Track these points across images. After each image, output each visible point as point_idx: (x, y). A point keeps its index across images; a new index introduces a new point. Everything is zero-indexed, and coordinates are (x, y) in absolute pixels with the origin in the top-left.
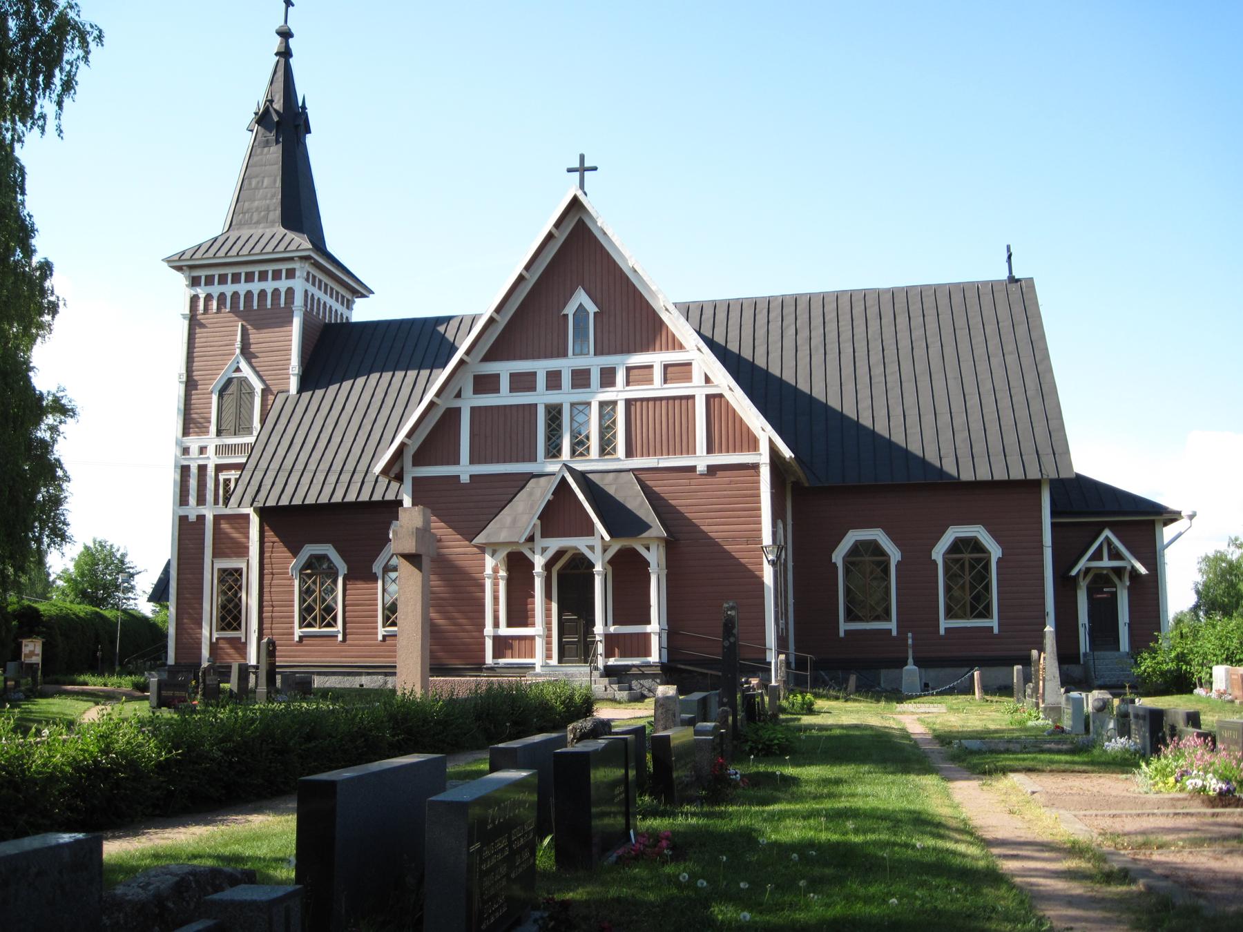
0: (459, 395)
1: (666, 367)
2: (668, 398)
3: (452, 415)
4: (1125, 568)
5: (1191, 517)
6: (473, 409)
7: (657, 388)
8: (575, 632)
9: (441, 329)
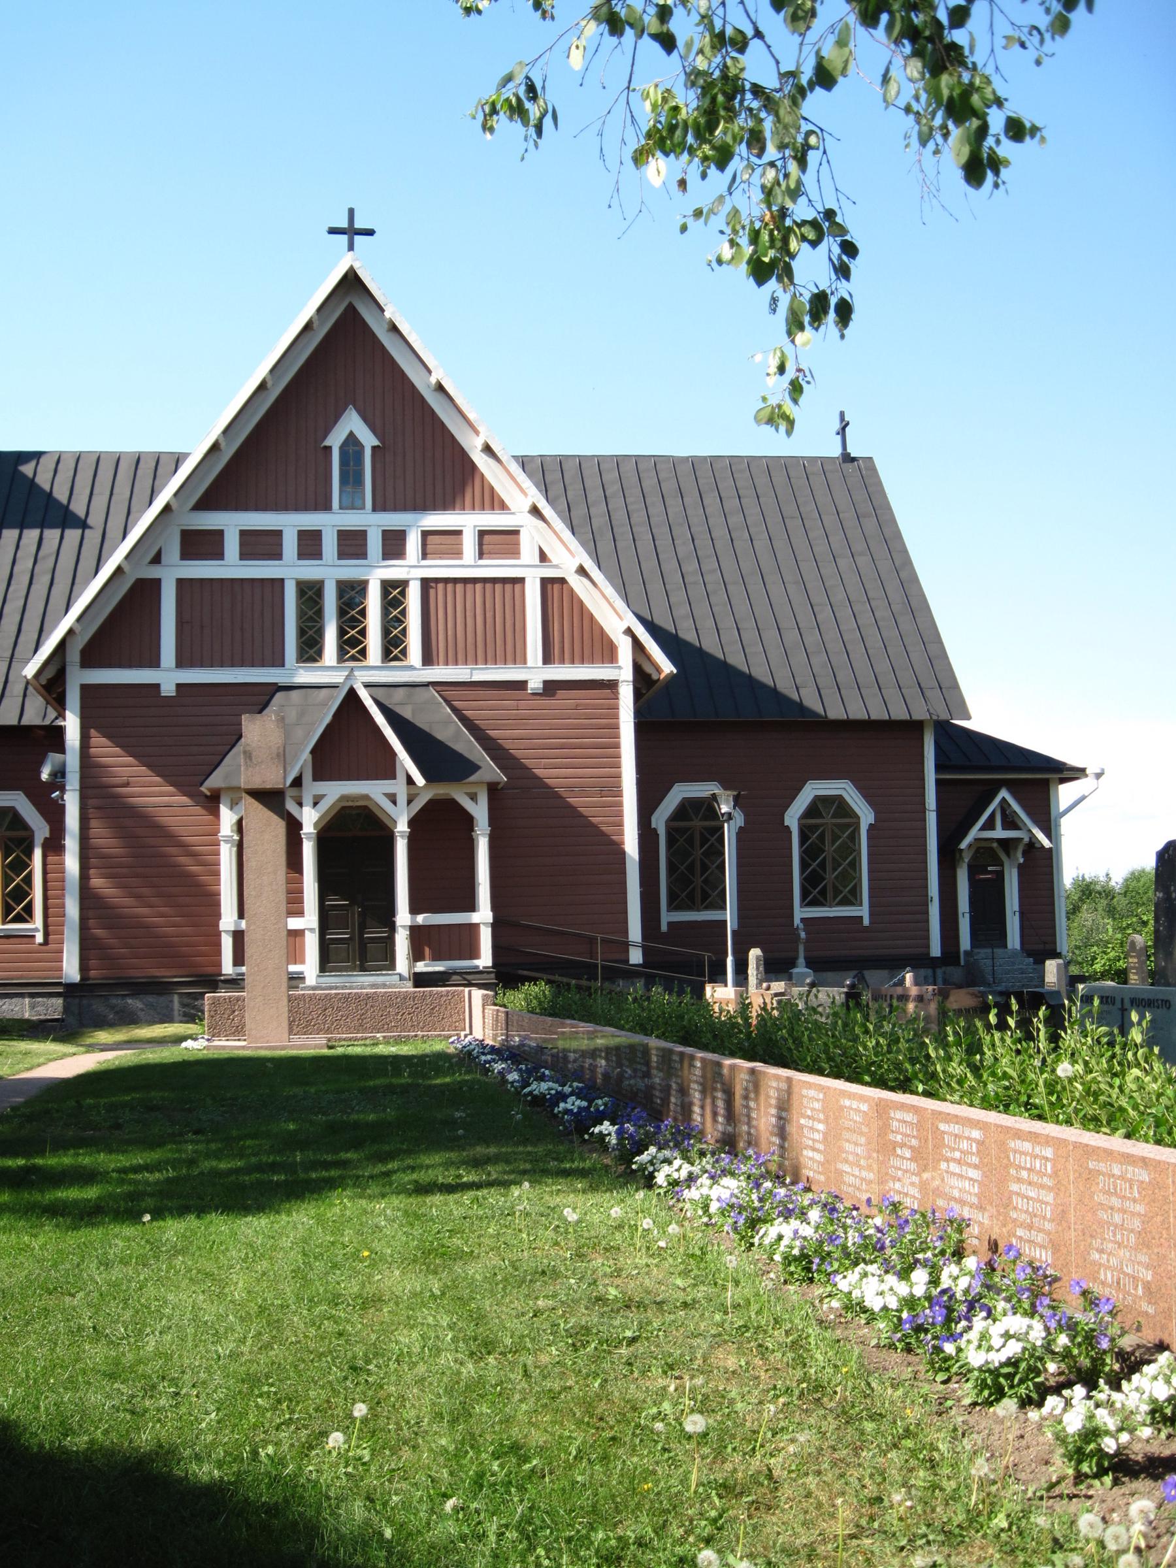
0: (157, 560)
1: (482, 534)
2: (485, 580)
3: (147, 590)
4: (1019, 840)
5: (1098, 776)
6: (181, 582)
7: (469, 564)
8: (342, 924)
9: (27, 469)
